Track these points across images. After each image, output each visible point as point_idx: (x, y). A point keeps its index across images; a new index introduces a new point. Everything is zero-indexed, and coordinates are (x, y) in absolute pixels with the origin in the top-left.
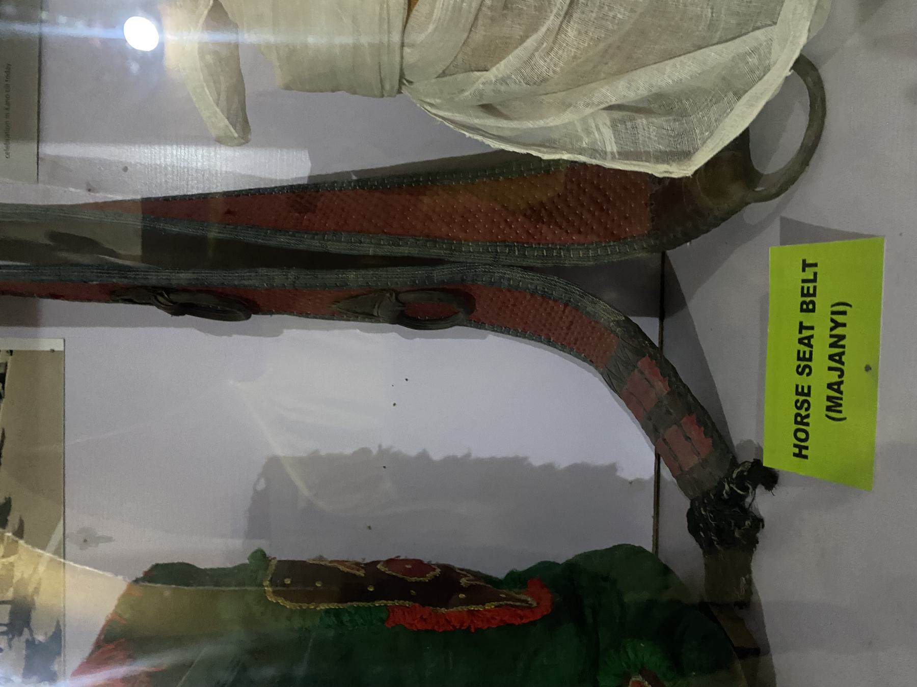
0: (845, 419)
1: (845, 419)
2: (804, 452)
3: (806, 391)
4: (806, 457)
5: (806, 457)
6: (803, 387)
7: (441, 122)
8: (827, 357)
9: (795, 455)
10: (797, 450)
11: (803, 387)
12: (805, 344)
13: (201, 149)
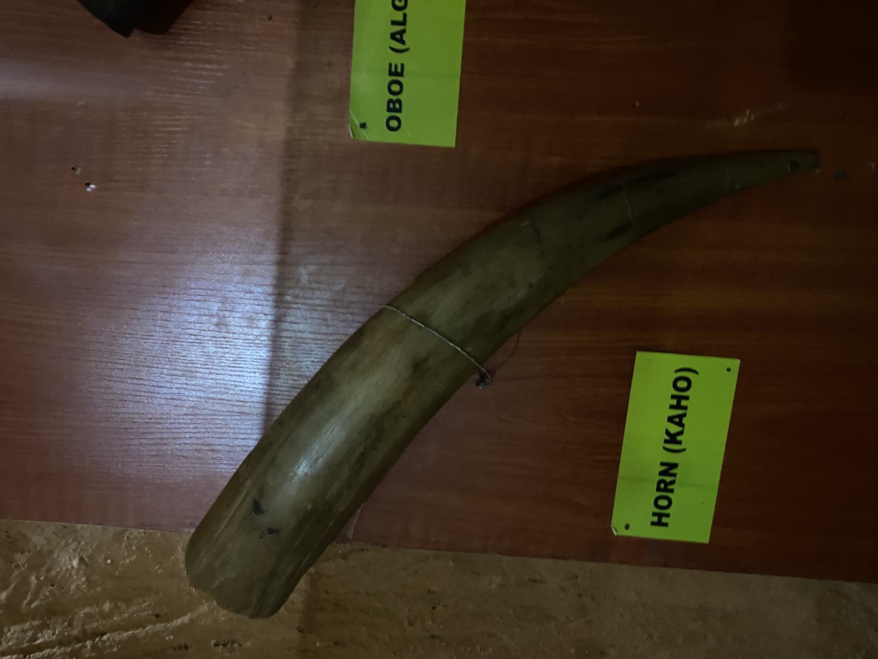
0: (684, 450)
1: (684, 450)
2: (664, 520)
3: (399, 70)
4: (666, 525)
5: (666, 525)
6: (396, 66)
7: (485, 373)
8: (389, 36)
9: (653, 524)
10: (656, 519)
11: (396, 66)
12: (676, 423)
13: (261, 432)
